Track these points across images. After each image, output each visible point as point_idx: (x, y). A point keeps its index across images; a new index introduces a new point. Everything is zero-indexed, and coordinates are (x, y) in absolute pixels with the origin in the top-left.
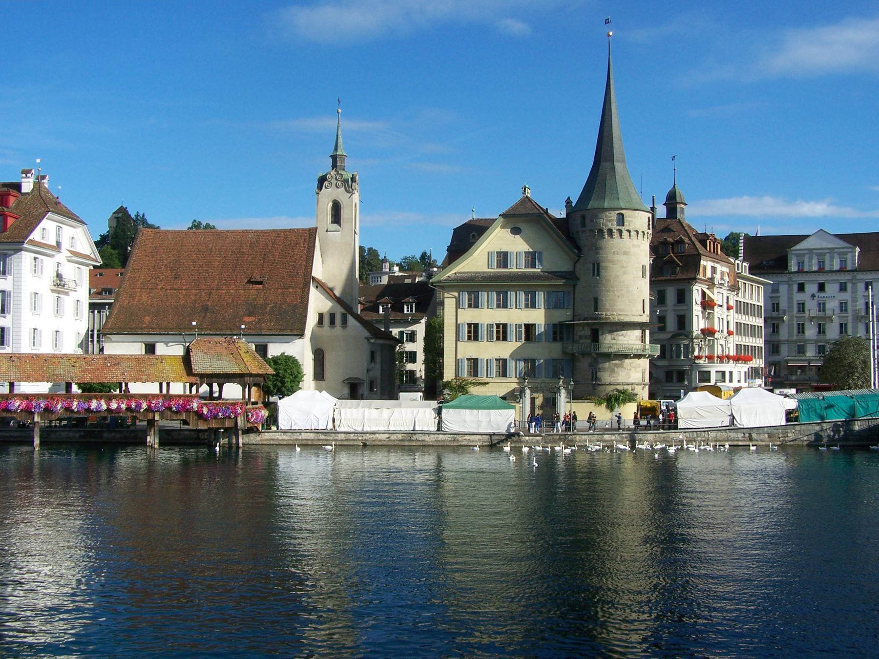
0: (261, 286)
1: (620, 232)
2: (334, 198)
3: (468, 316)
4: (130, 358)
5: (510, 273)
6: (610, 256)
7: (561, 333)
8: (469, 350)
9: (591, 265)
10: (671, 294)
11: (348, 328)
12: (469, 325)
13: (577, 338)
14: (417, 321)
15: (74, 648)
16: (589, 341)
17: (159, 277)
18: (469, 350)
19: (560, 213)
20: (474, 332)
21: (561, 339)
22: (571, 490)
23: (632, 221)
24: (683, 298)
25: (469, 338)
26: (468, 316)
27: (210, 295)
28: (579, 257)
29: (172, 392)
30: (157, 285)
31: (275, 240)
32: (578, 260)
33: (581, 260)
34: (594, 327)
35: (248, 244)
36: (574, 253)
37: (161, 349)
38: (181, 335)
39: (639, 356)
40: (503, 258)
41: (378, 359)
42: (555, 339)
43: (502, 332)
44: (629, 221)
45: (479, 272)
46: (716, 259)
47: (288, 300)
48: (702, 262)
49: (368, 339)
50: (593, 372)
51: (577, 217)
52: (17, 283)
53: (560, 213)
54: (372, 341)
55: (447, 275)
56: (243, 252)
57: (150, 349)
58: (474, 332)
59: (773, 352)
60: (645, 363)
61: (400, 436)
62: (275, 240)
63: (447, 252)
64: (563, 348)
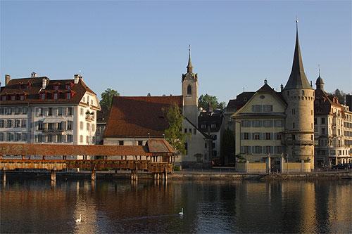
1: (303, 98)
3: (245, 130)
4: (116, 146)
6: (303, 113)
8: (245, 143)
10: (319, 119)
14: (217, 131)
18: (245, 143)
19: (279, 90)
20: (246, 136)
21: (280, 139)
24: (324, 121)
26: (245, 130)
29: (88, 159)
37: (126, 144)
39: (310, 145)
40: (258, 107)
41: (208, 146)
46: (337, 106)
48: (332, 107)
51: (286, 92)
52: (76, 118)
53: (279, 90)
55: (197, 99)
57: (121, 143)
58: (246, 136)
60: (313, 147)
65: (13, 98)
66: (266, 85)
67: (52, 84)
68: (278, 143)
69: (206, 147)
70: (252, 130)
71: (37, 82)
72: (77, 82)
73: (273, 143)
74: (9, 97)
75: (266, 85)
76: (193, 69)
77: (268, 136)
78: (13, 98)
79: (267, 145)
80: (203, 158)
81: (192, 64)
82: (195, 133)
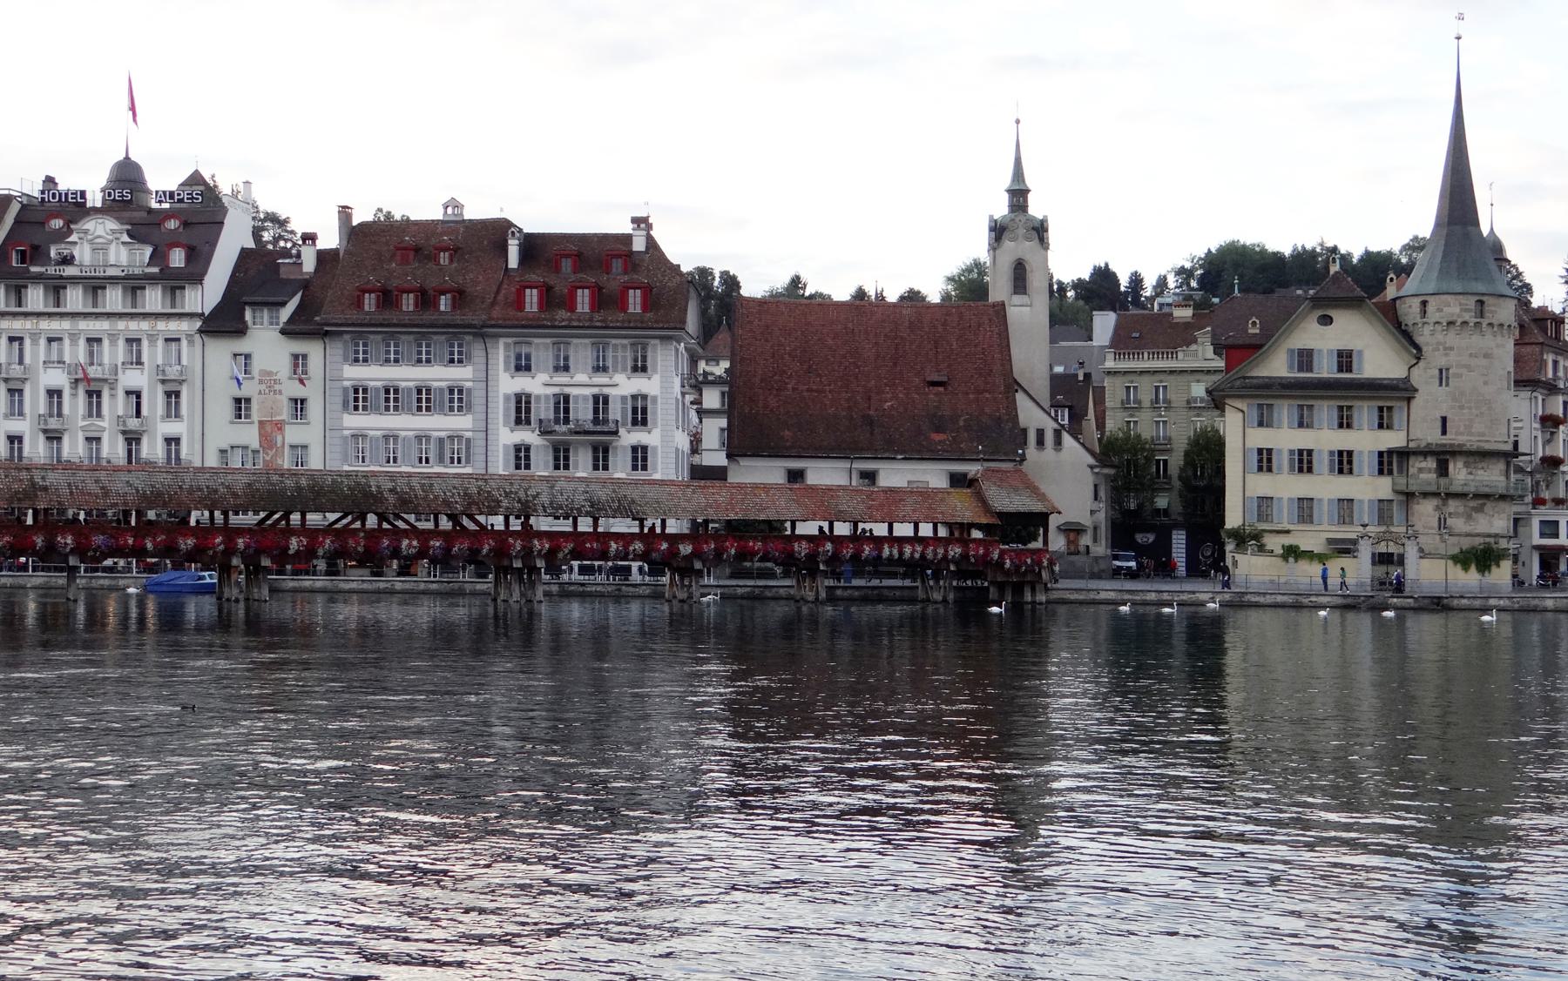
0: (941, 389)
2: (1020, 255)
3: (1261, 438)
5: (1319, 379)
7: (1390, 463)
8: (1262, 485)
9: (1437, 372)
11: (1064, 450)
12: (1260, 451)
13: (1412, 471)
15: (1441, 788)
16: (1435, 476)
17: (784, 372)
20: (1265, 460)
21: (1390, 473)
22: (1037, 706)
23: (1496, 312)
25: (1260, 469)
26: (1261, 438)
27: (869, 399)
28: (1419, 359)
30: (787, 384)
31: (946, 320)
32: (1417, 363)
33: (1420, 364)
34: (1442, 457)
35: (907, 324)
36: (1410, 353)
38: (849, 458)
41: (1102, 494)
42: (1381, 472)
43: (1344, 462)
44: (1491, 312)
45: (1275, 378)
47: (987, 410)
49: (1092, 467)
50: (1440, 519)
54: (1096, 470)
56: (902, 338)
58: (1265, 460)
59: (169, 416)
61: (1426, 601)
62: (946, 320)
63: (841, 293)
64: (1394, 484)
65: (408, 302)
66: (127, 158)
67: (534, 246)
68: (1383, 487)
69: (1096, 498)
70: (1285, 438)
71: (498, 231)
72: (639, 245)
73: (1368, 488)
74: (388, 298)
75: (127, 158)
76: (1032, 199)
77: (1344, 462)
78: (408, 302)
79: (634, 391)
80: (1086, 540)
81: (1030, 181)
82: (1058, 442)
